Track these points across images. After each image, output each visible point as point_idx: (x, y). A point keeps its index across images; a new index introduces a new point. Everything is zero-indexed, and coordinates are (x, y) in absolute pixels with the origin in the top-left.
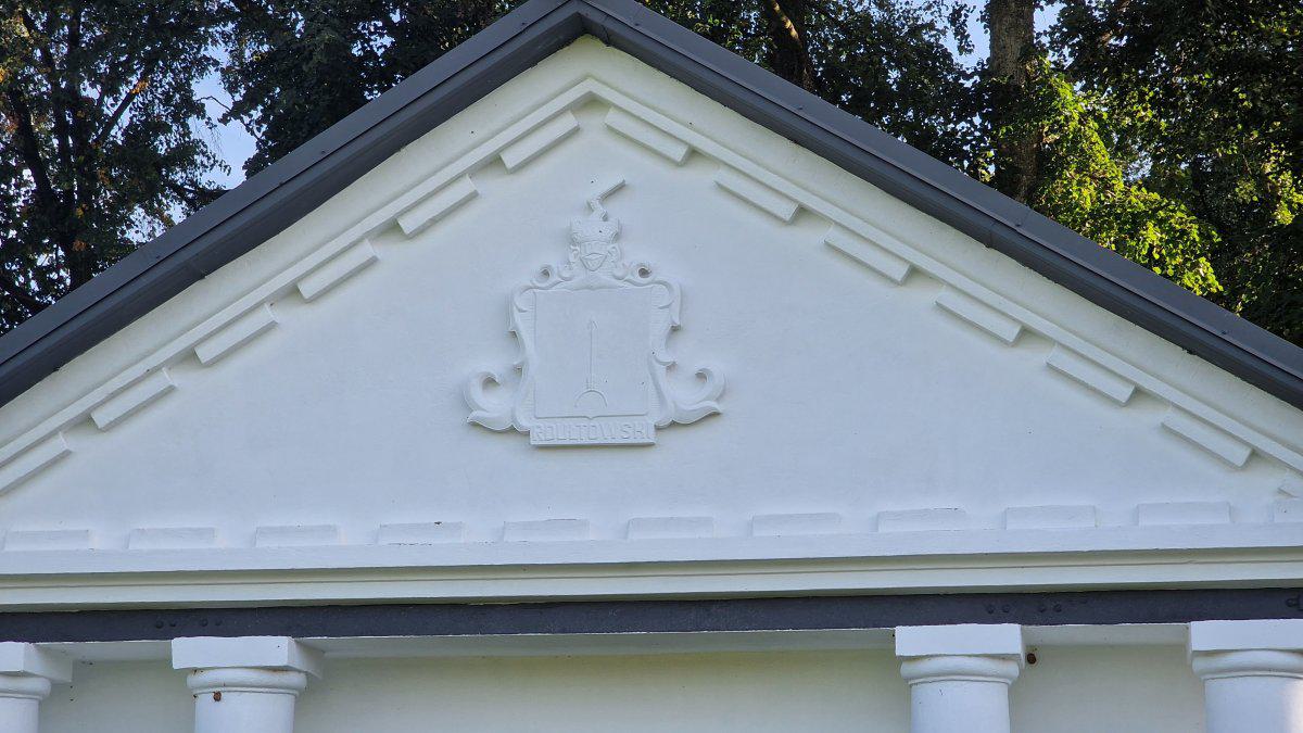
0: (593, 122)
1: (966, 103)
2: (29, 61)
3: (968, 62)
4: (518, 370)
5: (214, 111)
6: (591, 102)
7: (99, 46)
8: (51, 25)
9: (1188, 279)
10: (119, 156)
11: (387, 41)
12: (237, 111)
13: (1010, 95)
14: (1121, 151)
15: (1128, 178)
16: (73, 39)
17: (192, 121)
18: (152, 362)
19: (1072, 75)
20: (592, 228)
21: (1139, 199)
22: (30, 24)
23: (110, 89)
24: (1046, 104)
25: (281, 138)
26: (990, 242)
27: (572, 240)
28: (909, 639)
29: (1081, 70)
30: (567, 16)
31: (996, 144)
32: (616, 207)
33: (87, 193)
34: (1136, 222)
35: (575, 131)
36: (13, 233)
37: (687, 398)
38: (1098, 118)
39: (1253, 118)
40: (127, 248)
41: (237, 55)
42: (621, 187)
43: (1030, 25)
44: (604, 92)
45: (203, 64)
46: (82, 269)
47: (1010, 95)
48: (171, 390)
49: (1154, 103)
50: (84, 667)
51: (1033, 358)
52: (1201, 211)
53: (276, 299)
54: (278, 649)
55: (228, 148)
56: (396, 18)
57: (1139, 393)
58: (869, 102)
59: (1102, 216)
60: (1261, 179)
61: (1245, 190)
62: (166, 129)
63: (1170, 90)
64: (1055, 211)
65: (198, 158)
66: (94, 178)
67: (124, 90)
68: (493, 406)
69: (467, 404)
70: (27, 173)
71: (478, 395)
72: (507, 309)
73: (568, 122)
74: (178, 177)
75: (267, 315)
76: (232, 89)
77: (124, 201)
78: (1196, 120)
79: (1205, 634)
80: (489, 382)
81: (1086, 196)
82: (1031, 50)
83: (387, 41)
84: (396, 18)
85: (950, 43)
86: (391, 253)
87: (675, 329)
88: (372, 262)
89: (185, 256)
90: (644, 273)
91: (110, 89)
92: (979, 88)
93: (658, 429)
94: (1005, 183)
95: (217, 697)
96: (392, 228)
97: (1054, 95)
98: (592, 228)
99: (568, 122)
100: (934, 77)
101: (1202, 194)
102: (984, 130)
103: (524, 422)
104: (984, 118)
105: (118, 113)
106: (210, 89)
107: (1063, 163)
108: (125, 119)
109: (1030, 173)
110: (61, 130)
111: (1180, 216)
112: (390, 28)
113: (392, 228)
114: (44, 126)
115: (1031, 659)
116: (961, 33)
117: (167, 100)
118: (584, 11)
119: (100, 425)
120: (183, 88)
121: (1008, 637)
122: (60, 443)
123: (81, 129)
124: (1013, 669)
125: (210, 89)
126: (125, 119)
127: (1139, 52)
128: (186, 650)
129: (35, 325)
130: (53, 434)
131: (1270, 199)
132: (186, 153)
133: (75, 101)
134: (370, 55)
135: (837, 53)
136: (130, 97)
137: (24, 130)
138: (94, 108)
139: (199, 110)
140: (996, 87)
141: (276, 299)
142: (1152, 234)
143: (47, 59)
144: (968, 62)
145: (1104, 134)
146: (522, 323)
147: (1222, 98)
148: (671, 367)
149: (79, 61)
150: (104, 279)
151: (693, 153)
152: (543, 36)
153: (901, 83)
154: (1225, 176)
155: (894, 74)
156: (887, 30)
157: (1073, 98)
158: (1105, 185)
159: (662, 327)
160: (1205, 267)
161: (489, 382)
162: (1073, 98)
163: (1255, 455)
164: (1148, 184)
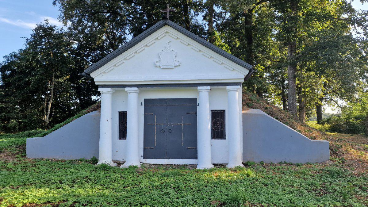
0: (167, 34)
1: (206, 34)
2: (108, 28)
3: (206, 29)
4: (160, 61)
5: (128, 34)
6: (167, 32)
7: (115, 27)
8: (110, 24)
9: (228, 52)
10: (118, 38)
11: (146, 26)
12: (130, 34)
13: (210, 33)
14: (221, 39)
15: (222, 42)
16: (113, 26)
17: (126, 35)
18: (122, 59)
19: (217, 31)
20: (167, 46)
21: (223, 44)
22: (108, 24)
23: (117, 31)
24: (214, 34)
25: (135, 35)
26: (208, 47)
27: (165, 47)
28: (199, 88)
29: (218, 30)
30: (218, 87)
31: (209, 38)
32: (169, 44)
33: (115, 43)
34: (223, 46)
35: (165, 35)
36: (28, 63)
37: (177, 64)
38: (219, 35)
39: (235, 35)
40: (118, 48)
41: (130, 28)
42: (170, 41)
43: (212, 26)
44: (169, 31)
45: (126, 29)
46: (114, 50)
47: (210, 33)
48: (124, 62)
49: (225, 34)
50: (116, 90)
51: (212, 59)
52: (229, 45)
53: (135, 53)
54: (136, 89)
55: (129, 37)
56: (147, 24)
57: (211, 57)
58: (196, 33)
59: (219, 46)
60: (235, 42)
61: (234, 43)
62: (123, 36)
63: (227, 32)
64: (215, 45)
65: (126, 39)
66: (115, 41)
67: (118, 31)
68: (158, 64)
69: (155, 64)
70: (108, 40)
71: (156, 63)
72: (159, 54)
73: (165, 34)
74: (124, 41)
75: (134, 54)
76: (129, 31)
77: (119, 43)
78: (229, 36)
79: (228, 87)
80: (157, 62)
81: (218, 44)
82: (212, 28)
83: (146, 26)
84: (147, 24)
85: (204, 27)
86: (146, 48)
87: (176, 57)
88: (145, 49)
89: (125, 48)
90: (173, 51)
91: (117, 31)
92: (207, 32)
93: (174, 67)
94: (210, 42)
95: (130, 94)
96: (146, 45)
97: (215, 33)
98: (167, 46)
99: (165, 34)
100: (203, 31)
101: (229, 43)
102: (208, 37)
103: (161, 66)
104: (208, 35)
105: (118, 34)
106: (127, 31)
107: (216, 40)
108: (118, 34)
109: (212, 41)
110: (112, 35)
111: (227, 46)
112: (146, 25)
113: (146, 45)
114: (110, 35)
115: (211, 90)
116: (205, 26)
117: (123, 33)
118: (166, 22)
119: (117, 66)
120: (124, 31)
121: (209, 88)
122: (113, 68)
123: (114, 36)
124: (209, 91)
125: (127, 31)
126: (118, 34)
127: (223, 29)
128: (127, 89)
129: (107, 57)
130: (112, 67)
131: (236, 44)
132: (125, 38)
133: (113, 33)
134: (144, 28)
135: (193, 28)
136: (119, 32)
137: (108, 35)
138: (115, 33)
139: (126, 34)
140: (209, 32)
141: (135, 53)
142: (224, 48)
143: (110, 28)
144: (206, 29)
145: (220, 37)
146: (160, 56)
147: (232, 33)
148: (175, 60)
149: (113, 28)
150: (116, 51)
151: (178, 38)
152: (161, 25)
153: (199, 32)
154: (231, 42)
155: (199, 31)
156: (198, 26)
157: (217, 33)
158: (220, 43)
159: (174, 56)
160: (229, 51)
161: (157, 62)
162: (217, 33)
163: (234, 69)
164: (224, 42)
